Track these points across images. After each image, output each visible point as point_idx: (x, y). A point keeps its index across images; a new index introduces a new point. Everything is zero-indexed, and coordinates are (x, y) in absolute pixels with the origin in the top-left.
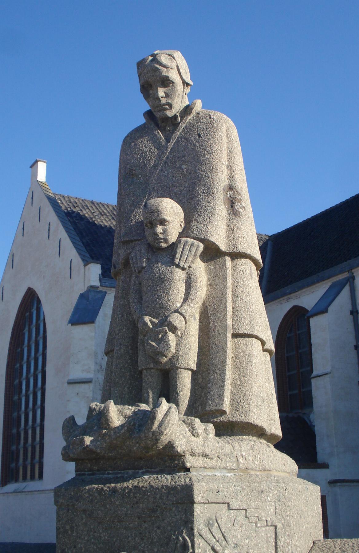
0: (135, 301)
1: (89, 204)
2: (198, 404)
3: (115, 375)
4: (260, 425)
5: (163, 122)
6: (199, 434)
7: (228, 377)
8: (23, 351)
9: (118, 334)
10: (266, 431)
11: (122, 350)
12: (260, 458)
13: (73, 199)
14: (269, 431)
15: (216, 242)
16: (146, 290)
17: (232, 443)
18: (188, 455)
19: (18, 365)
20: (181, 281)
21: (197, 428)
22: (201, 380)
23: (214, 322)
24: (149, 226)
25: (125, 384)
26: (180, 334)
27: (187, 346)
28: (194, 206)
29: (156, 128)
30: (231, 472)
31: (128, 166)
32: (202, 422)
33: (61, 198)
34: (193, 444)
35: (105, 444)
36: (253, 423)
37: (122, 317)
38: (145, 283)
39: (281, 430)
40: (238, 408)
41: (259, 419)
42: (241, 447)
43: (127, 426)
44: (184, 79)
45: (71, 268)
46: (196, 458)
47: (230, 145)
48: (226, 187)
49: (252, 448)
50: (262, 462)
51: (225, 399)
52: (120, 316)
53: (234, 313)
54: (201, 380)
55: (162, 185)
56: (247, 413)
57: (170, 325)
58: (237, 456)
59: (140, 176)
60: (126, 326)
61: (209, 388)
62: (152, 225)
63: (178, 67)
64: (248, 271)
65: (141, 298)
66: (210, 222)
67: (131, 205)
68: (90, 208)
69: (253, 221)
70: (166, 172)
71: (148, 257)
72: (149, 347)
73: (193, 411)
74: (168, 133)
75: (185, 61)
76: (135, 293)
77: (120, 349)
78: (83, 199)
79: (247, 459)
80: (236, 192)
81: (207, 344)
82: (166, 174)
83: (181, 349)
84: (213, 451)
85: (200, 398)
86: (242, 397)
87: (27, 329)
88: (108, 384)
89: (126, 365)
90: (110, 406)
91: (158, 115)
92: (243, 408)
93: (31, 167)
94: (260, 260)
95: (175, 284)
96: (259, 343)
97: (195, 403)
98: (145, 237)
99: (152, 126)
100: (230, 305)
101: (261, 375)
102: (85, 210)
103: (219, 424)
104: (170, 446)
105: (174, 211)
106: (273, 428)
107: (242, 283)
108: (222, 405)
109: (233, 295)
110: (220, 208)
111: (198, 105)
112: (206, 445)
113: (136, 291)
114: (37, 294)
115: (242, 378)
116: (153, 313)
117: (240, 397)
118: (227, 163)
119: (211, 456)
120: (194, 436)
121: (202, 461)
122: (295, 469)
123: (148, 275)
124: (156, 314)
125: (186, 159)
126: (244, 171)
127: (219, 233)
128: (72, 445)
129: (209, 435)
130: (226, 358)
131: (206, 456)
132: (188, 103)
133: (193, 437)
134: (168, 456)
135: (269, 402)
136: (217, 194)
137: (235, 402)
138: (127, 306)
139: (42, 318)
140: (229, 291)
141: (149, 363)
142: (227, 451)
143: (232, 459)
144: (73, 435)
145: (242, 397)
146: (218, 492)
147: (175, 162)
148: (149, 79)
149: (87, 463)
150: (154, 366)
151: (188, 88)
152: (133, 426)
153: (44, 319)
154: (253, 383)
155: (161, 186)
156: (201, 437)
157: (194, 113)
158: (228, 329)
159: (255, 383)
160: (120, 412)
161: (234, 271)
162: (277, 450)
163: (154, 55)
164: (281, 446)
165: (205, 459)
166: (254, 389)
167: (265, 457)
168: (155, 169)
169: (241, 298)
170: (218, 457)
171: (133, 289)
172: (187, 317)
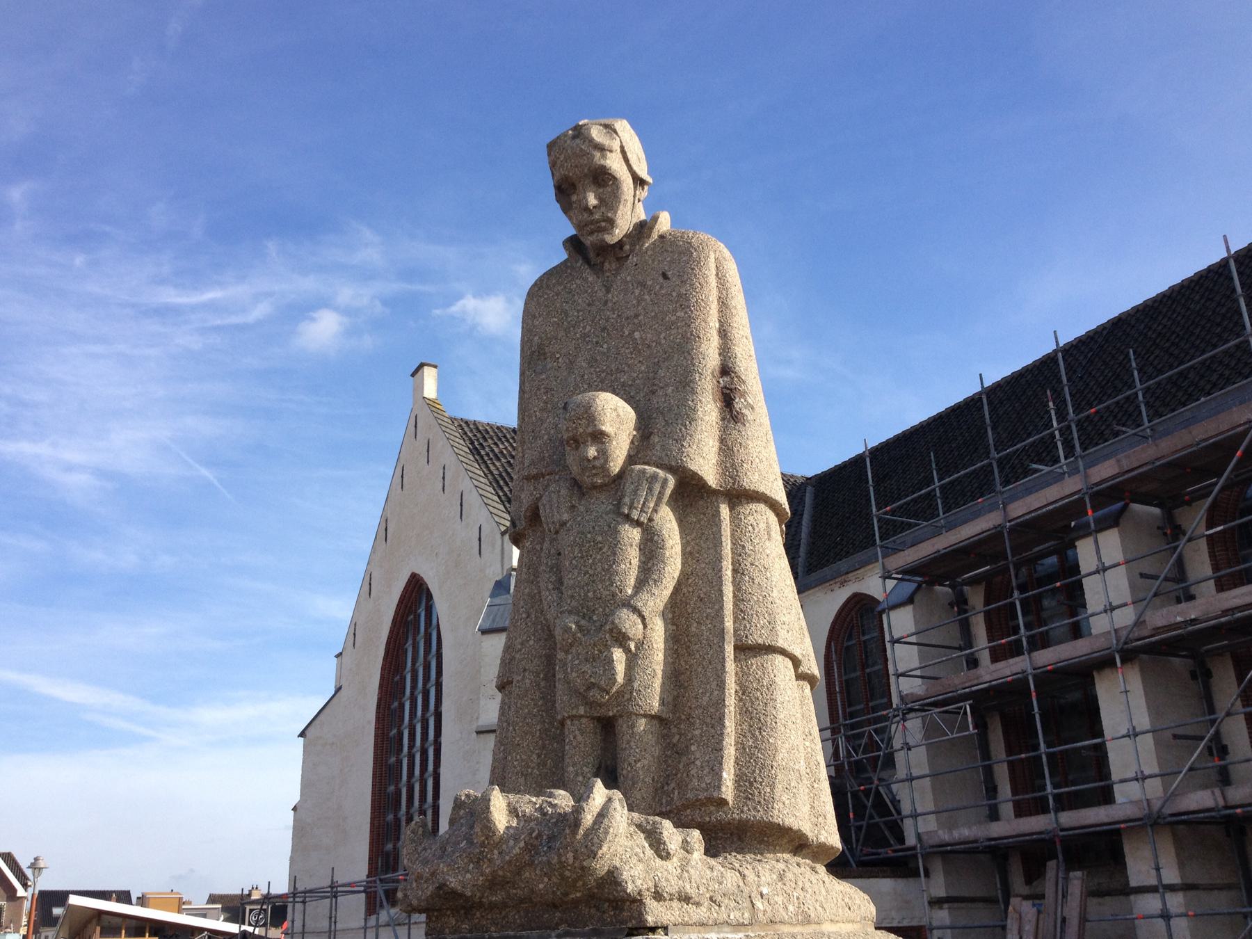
0: (551, 586)
1: (509, 433)
2: (673, 785)
3: (515, 730)
4: (795, 828)
5: (598, 255)
6: (672, 852)
7: (729, 730)
8: (403, 679)
9: (520, 650)
10: (808, 839)
11: (527, 681)
12: (798, 898)
13: (483, 426)
14: (815, 839)
15: (699, 472)
16: (569, 565)
17: (741, 869)
18: (648, 899)
19: (396, 704)
20: (634, 547)
21: (667, 841)
24: (574, 446)
26: (633, 649)
28: (656, 406)
29: (586, 267)
30: (740, 931)
31: (536, 338)
32: (676, 826)
33: (463, 425)
34: (659, 875)
35: (481, 878)
36: (781, 823)
38: (567, 553)
39: (838, 836)
40: (751, 794)
42: (759, 876)
43: (524, 839)
44: (635, 172)
45: (480, 539)
46: (666, 903)
48: (717, 368)
49: (781, 877)
50: (802, 905)
51: (725, 775)
52: (524, 616)
53: (737, 605)
54: (677, 737)
55: (598, 370)
56: (768, 803)
57: (615, 631)
58: (750, 897)
59: (558, 356)
60: (534, 635)
61: (693, 753)
62: (577, 442)
63: (622, 148)
64: (762, 526)
65: (560, 581)
67: (542, 410)
68: (511, 441)
69: (771, 432)
70: (605, 346)
73: (664, 801)
74: (608, 274)
75: (637, 138)
76: (550, 572)
78: (498, 425)
79: (772, 901)
80: (736, 379)
82: (605, 350)
83: (637, 677)
84: (701, 888)
85: (676, 775)
86: (757, 771)
87: (410, 642)
88: (502, 748)
90: (492, 798)
91: (589, 242)
92: (760, 793)
93: (413, 375)
94: (786, 506)
96: (790, 664)
97: (667, 784)
98: (566, 467)
99: (579, 265)
100: (728, 590)
101: (794, 726)
102: (503, 443)
103: (715, 826)
104: (612, 878)
105: (618, 416)
106: (823, 832)
108: (719, 787)
109: (735, 571)
110: (706, 409)
111: (665, 223)
112: (686, 875)
113: (552, 568)
114: (426, 583)
115: (757, 733)
117: (754, 771)
118: (717, 325)
120: (662, 859)
122: (871, 913)
124: (588, 610)
125: (640, 321)
126: (751, 340)
127: (704, 455)
128: (416, 881)
129: (692, 853)
130: (724, 693)
131: (685, 899)
132: (643, 217)
133: (658, 860)
134: (608, 900)
135: (813, 780)
136: (699, 383)
137: (744, 781)
139: (434, 622)
140: (725, 563)
141: (577, 707)
142: (729, 885)
143: (740, 902)
144: (420, 859)
145: (757, 771)
147: (622, 327)
148: (569, 172)
149: (449, 916)
150: (585, 712)
151: (643, 189)
152: (536, 838)
153: (438, 625)
154: (779, 743)
155: (596, 373)
156: (675, 859)
157: (655, 235)
158: (726, 637)
159: (783, 743)
160: (513, 811)
161: (736, 526)
162: (831, 877)
164: (840, 867)
165: (685, 906)
166: (781, 755)
167: (808, 896)
168: (584, 340)
169: (750, 577)
170: (712, 901)
171: (547, 564)
172: (646, 615)
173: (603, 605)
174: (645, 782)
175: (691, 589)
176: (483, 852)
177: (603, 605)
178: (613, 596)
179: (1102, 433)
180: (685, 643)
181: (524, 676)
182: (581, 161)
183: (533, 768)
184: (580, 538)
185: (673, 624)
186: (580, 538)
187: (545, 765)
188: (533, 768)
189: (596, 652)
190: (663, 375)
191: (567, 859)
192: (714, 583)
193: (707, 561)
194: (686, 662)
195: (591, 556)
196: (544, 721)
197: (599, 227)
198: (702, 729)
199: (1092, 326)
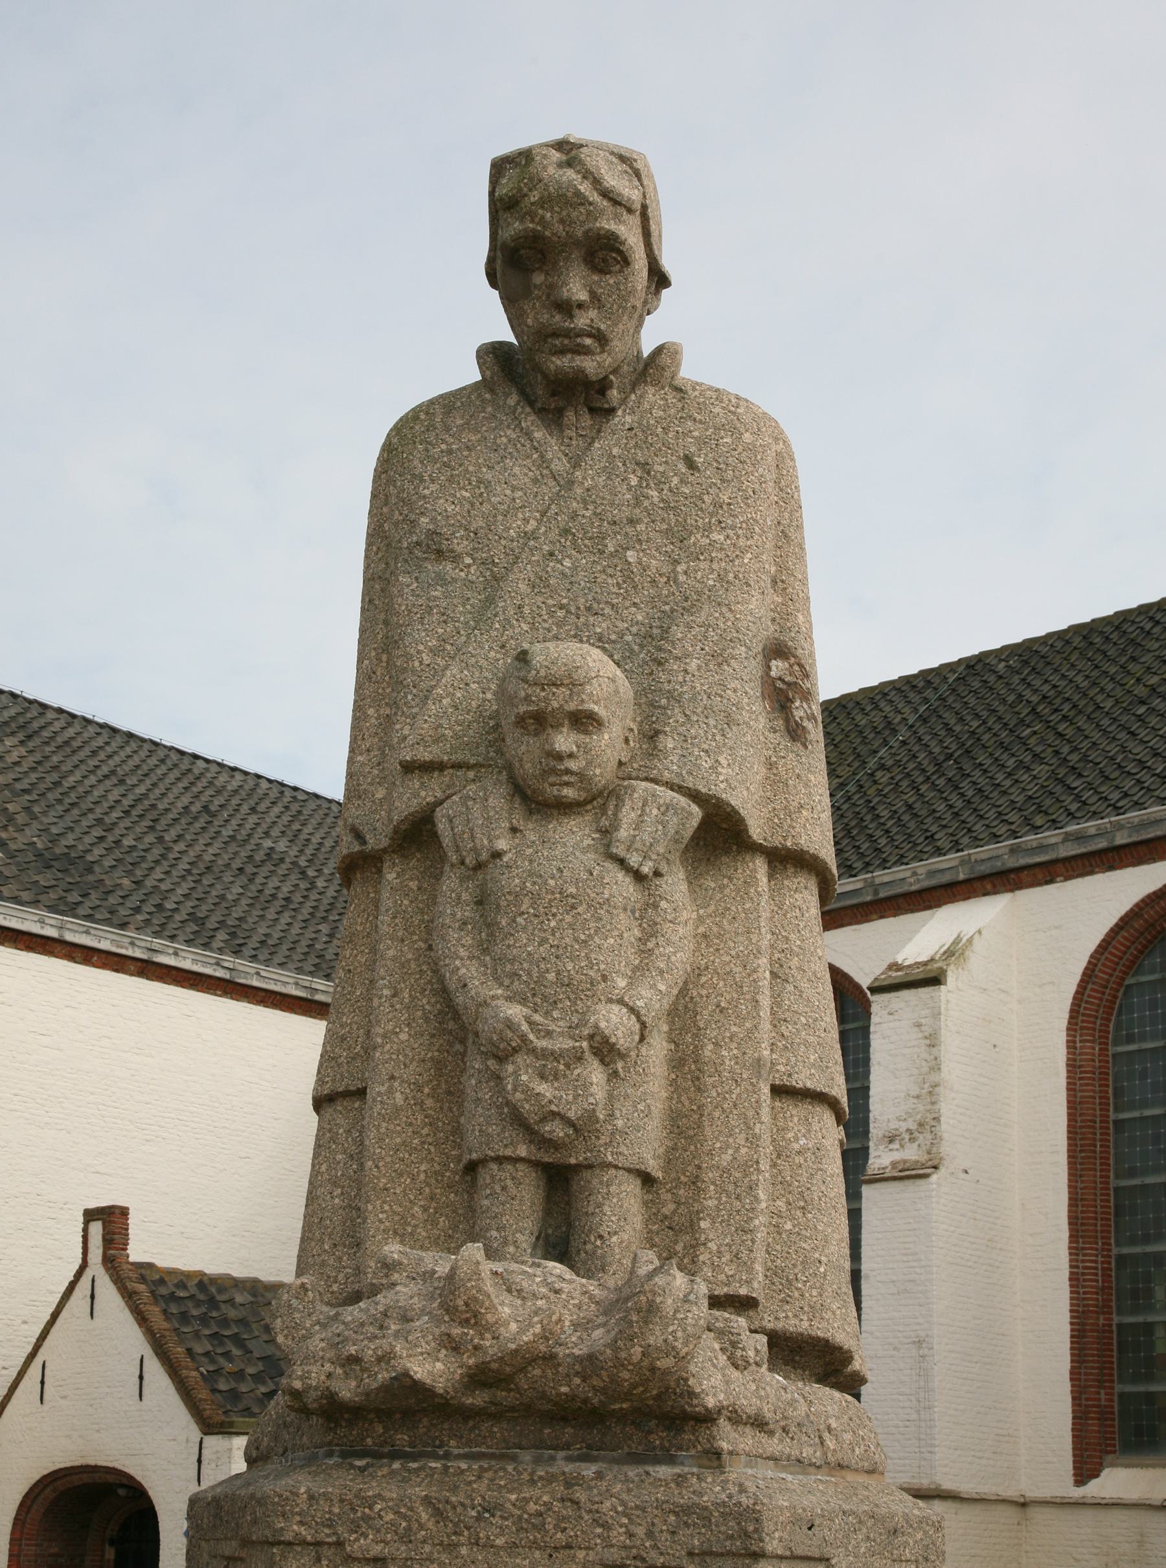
11: (398, 1095)
15: (741, 811)
22: (672, 1206)
23: (716, 1044)
25: (412, 1198)
27: (640, 1107)
29: (528, 409)
37: (394, 996)
41: (844, 1330)
47: (786, 515)
54: (672, 1206)
55: (550, 602)
59: (468, 560)
60: (408, 1025)
66: (725, 744)
67: (434, 651)
70: (567, 563)
71: (511, 823)
72: (523, 1096)
77: (391, 1091)
81: (694, 1107)
89: (415, 1141)
95: (612, 918)
107: (798, 943)
116: (534, 995)
119: (771, 1426)
120: (737, 1367)
121: (753, 1437)
123: (517, 881)
133: (732, 1369)
138: (413, 966)
146: (810, 1529)
149: (372, 1422)
163: (568, 147)
173: (572, 996)
174: (622, 1264)
175: (704, 992)
176: (467, 1334)
177: (572, 996)
178: (592, 984)
179: (932, 836)
180: (690, 1071)
181: (391, 1087)
182: (574, 214)
183: (416, 1226)
184: (534, 883)
185: (672, 1041)
186: (534, 883)
187: (435, 1223)
188: (416, 1226)
189: (562, 1067)
190: (680, 635)
191: (630, 1355)
192: (745, 989)
193: (733, 953)
194: (691, 1101)
195: (554, 915)
196: (433, 1159)
197: (579, 345)
198: (719, 1199)
199: (933, 661)
